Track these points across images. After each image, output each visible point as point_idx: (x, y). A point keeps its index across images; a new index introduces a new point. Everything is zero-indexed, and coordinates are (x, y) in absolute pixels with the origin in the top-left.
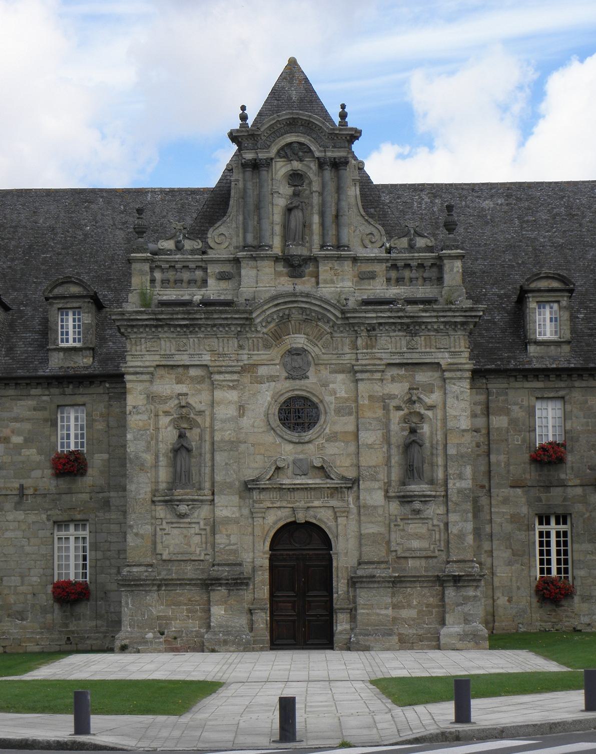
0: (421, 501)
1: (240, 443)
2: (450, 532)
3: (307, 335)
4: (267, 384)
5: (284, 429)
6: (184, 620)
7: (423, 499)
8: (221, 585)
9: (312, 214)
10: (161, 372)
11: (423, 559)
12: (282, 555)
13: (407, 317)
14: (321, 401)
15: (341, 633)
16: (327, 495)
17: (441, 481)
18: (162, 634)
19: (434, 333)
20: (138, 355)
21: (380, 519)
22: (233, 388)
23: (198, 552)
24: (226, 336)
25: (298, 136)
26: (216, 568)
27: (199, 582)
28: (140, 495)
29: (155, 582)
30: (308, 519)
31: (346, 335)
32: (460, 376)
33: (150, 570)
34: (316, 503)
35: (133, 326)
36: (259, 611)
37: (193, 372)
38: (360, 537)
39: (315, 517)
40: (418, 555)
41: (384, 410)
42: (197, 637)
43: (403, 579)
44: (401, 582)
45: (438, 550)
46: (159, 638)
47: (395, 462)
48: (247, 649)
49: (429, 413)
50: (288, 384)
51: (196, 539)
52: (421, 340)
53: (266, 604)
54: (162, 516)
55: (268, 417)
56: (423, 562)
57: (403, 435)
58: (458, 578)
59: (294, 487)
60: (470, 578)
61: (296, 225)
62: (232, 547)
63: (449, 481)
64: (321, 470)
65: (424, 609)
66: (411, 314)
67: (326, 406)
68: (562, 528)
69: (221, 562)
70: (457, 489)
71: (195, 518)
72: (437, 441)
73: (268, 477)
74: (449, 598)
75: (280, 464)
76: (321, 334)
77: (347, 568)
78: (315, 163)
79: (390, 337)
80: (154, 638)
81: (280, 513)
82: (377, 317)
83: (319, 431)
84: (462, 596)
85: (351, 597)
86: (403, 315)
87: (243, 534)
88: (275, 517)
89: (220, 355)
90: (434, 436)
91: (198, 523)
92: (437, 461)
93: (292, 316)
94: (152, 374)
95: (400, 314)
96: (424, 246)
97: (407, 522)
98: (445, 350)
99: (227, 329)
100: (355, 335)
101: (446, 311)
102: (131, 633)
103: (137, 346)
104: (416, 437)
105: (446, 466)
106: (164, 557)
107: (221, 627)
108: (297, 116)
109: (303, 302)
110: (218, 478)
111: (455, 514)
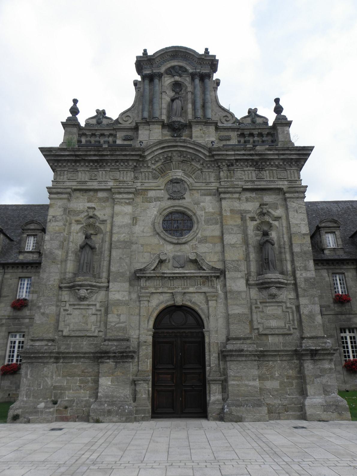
0: (277, 287)
1: (132, 244)
2: (301, 312)
3: (184, 171)
4: (155, 203)
5: (166, 234)
6: (77, 390)
7: (278, 285)
8: (109, 358)
9: (187, 104)
10: (78, 194)
11: (281, 336)
12: (163, 333)
13: (257, 155)
14: (195, 214)
15: (214, 403)
16: (200, 283)
17: (290, 272)
18: (55, 403)
19: (276, 169)
20: (61, 182)
21: (243, 302)
22: (129, 204)
23: (93, 329)
24: (126, 169)
25: (179, 62)
26: (106, 343)
27: (91, 355)
28: (49, 282)
29: (52, 355)
30: (184, 302)
31: (212, 171)
33: (50, 344)
34: (191, 289)
36: (142, 382)
37: (100, 195)
38: (228, 317)
39: (191, 301)
40: (277, 332)
41: (242, 221)
42: (85, 406)
43: (265, 353)
44: (264, 356)
45: (293, 329)
46: (50, 408)
47: (253, 258)
49: (276, 223)
50: (170, 203)
51: (93, 319)
52: (266, 174)
53: (149, 376)
54: (66, 299)
55: (154, 226)
56: (281, 339)
57: (256, 239)
59: (173, 275)
60: (325, 352)
61: (177, 107)
62: (120, 325)
63: (297, 272)
67: (198, 217)
69: (111, 338)
72: (284, 242)
73: (153, 268)
74: (308, 370)
75: (163, 257)
76: (194, 171)
77: (218, 343)
78: (189, 78)
79: (244, 171)
80: (45, 407)
81: (162, 298)
82: (234, 155)
83: (193, 235)
84: (319, 368)
85: (222, 370)
87: (132, 315)
88: (158, 301)
89: (121, 182)
90: (282, 239)
91: (95, 305)
92: (285, 257)
93: (173, 158)
94: (69, 194)
95: (252, 152)
96: (262, 122)
97: (265, 304)
99: (126, 164)
100: (218, 171)
101: (285, 150)
102: (26, 402)
103: (61, 176)
104: (268, 238)
105: (293, 262)
106: (64, 334)
107: (107, 397)
108: (178, 49)
109: (181, 146)
110: (113, 269)
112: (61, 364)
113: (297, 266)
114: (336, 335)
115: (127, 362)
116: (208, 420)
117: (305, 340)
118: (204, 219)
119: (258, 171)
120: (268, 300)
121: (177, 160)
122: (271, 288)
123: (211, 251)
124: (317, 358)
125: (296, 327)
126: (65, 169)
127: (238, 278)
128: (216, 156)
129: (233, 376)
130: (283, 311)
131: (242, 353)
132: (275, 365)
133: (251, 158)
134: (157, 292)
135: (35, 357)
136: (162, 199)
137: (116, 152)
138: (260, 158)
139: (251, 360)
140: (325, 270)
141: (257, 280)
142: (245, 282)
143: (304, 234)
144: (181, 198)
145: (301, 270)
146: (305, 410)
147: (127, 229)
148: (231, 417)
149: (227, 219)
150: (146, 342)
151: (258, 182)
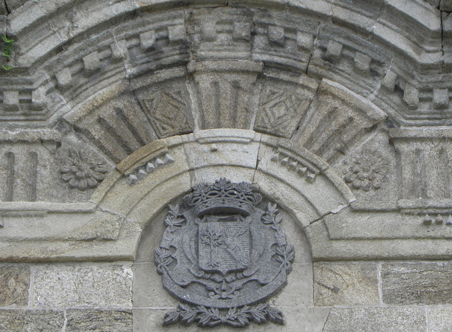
121: (224, 65)
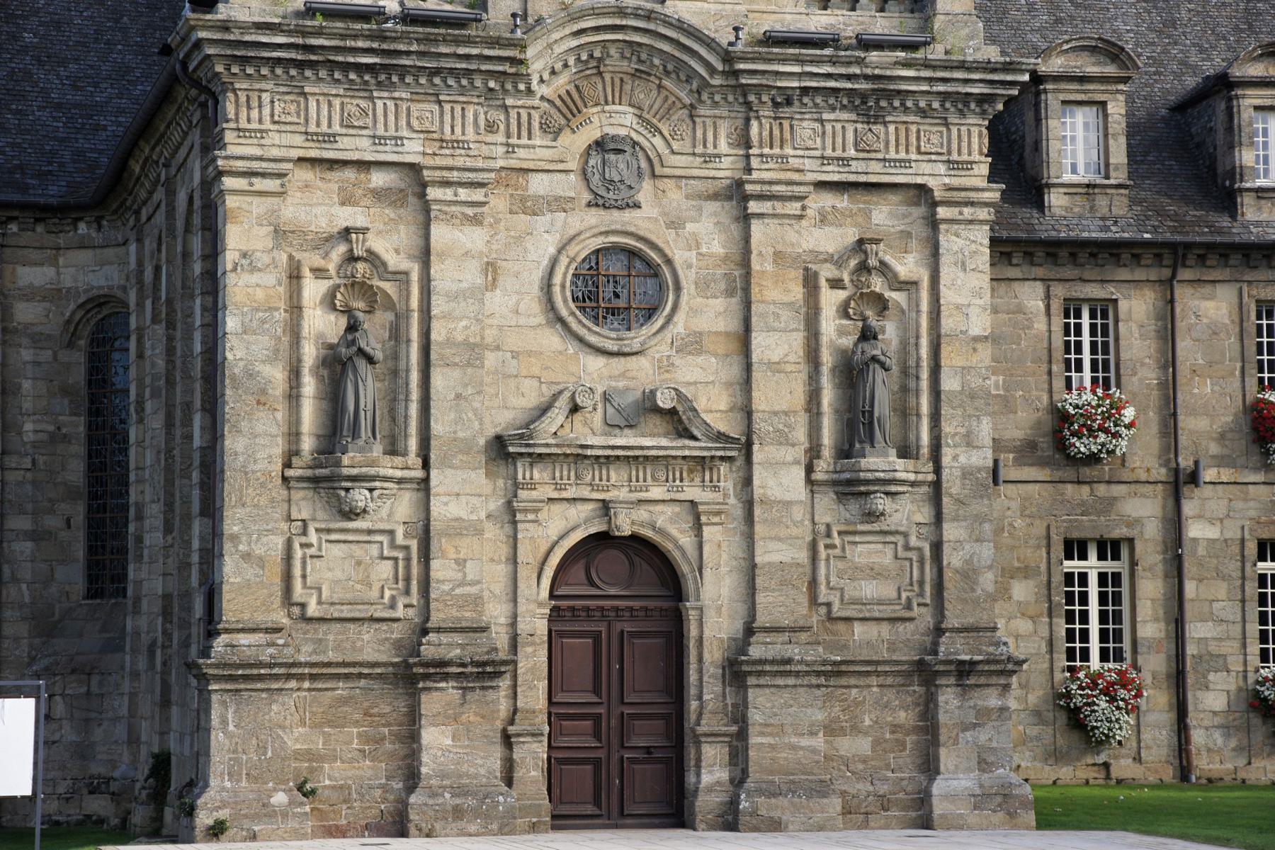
2: (945, 563)
3: (639, 108)
4: (549, 216)
8: (446, 677)
15: (710, 789)
19: (918, 119)
20: (255, 131)
21: (794, 531)
22: (476, 221)
31: (726, 114)
32: (970, 218)
33: (281, 642)
35: (244, 60)
36: (528, 739)
37: (379, 179)
40: (877, 615)
43: (843, 668)
44: (840, 674)
46: (302, 804)
48: (506, 829)
50: (595, 218)
52: (887, 133)
56: (885, 628)
58: (967, 667)
60: (993, 668)
62: (468, 589)
64: (668, 417)
65: (888, 736)
66: (877, 72)
68: (1110, 566)
70: (962, 468)
71: (382, 520)
82: (800, 75)
84: (974, 707)
85: (730, 708)
86: (858, 71)
88: (564, 522)
90: (912, 349)
92: (918, 404)
97: (850, 538)
98: (940, 158)
99: (464, 82)
101: (952, 68)
105: (936, 417)
107: (443, 775)
109: (636, 29)
111: (956, 524)
112: (304, 694)
113: (946, 434)
114: (1043, 566)
115: (492, 687)
116: (695, 829)
117: (947, 634)
118: (694, 276)
119: (862, 122)
120: (861, 527)
121: (617, 69)
122: (872, 496)
123: (711, 379)
124: (972, 681)
125: (928, 601)
126: (263, 85)
127: (784, 464)
128: (745, 76)
129: (761, 724)
130: (896, 558)
131: (788, 668)
132: (864, 697)
133: (849, 85)
134: (561, 497)
135: (246, 678)
136: (570, 205)
137: (438, 46)
138: (876, 87)
139: (808, 686)
140: (1038, 283)
141: (836, 472)
142: (803, 474)
143: (976, 339)
144: (628, 205)
145: (955, 446)
146: (931, 806)
147: (473, 304)
148: (754, 822)
149: (764, 283)
150: (531, 635)
151: (860, 162)
